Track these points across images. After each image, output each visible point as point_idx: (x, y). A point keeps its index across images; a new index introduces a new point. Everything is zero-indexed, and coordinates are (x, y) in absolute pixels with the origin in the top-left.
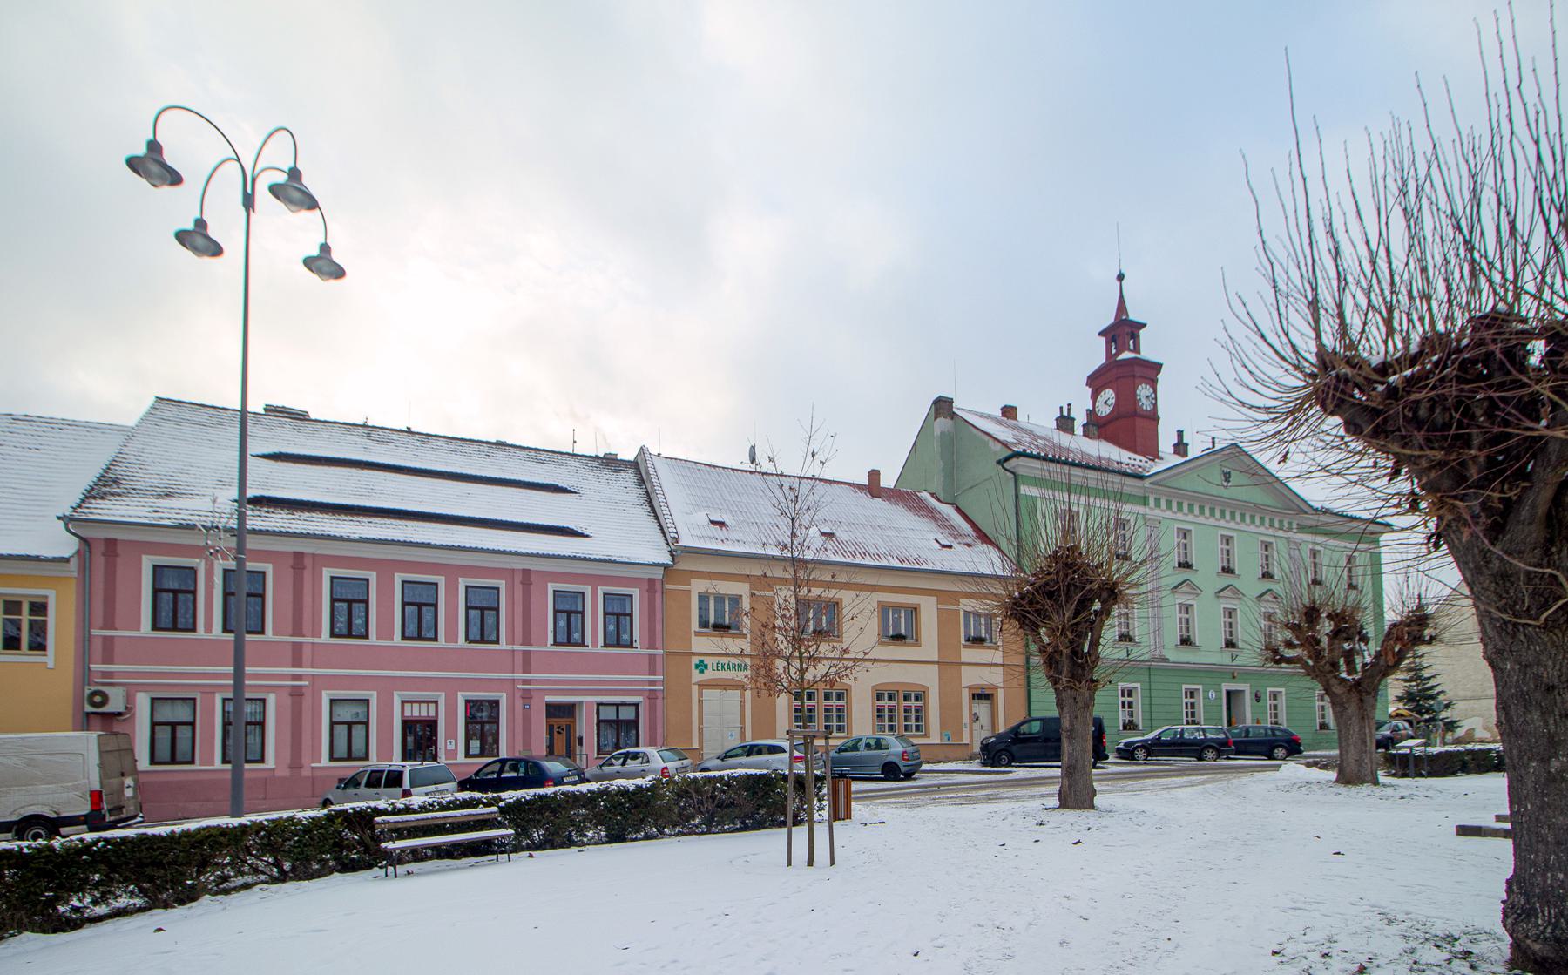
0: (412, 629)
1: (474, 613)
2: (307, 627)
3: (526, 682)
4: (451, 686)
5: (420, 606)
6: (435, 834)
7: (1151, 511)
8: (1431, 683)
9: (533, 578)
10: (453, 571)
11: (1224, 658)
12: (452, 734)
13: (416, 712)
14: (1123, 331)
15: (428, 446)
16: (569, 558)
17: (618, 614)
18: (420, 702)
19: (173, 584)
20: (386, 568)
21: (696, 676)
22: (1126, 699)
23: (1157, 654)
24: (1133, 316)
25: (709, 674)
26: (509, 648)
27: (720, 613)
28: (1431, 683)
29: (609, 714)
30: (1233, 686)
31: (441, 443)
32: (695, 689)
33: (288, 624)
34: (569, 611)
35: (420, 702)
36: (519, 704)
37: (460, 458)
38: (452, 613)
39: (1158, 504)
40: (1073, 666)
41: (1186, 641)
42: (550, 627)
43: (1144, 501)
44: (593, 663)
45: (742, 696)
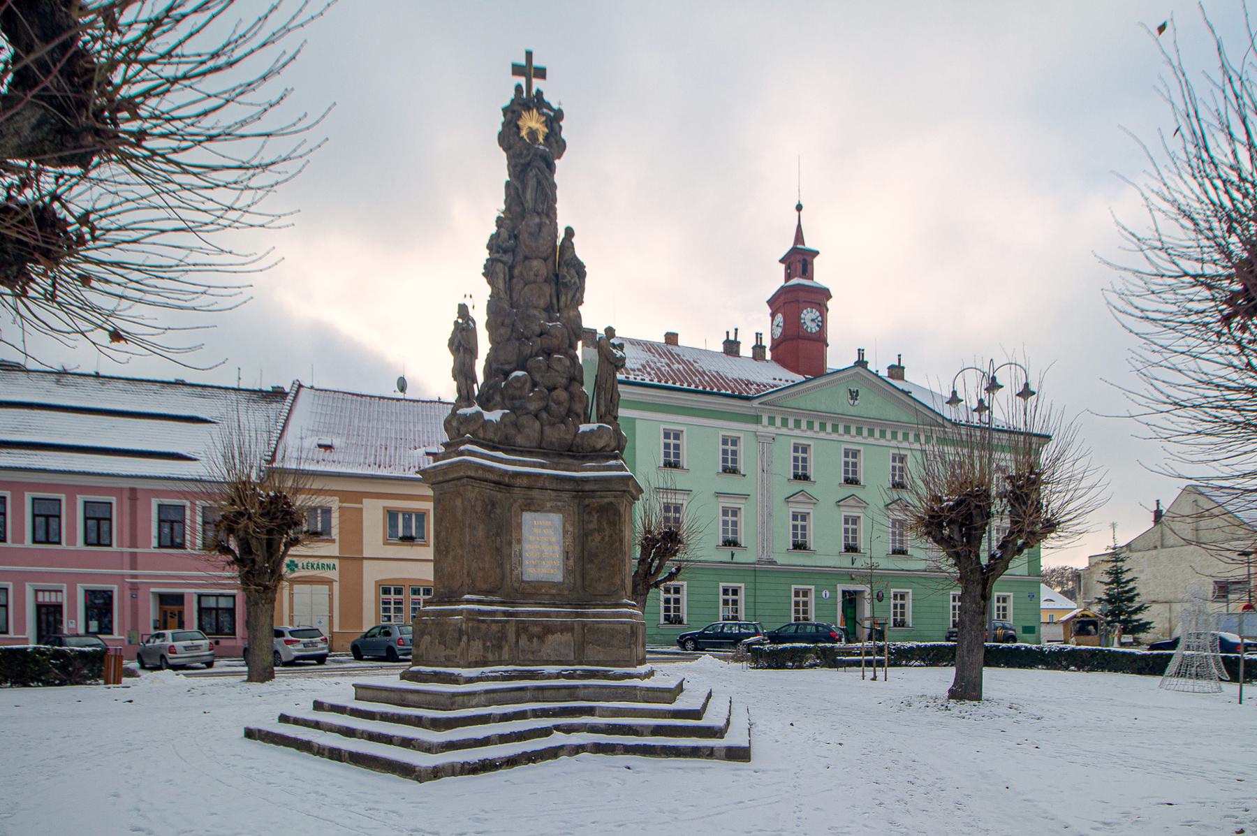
1: (40, 520)
4: (72, 579)
5: (99, 520)
6: (676, 727)
7: (764, 429)
8: (1131, 585)
9: (139, 495)
10: (72, 490)
11: (845, 561)
12: (73, 616)
14: (799, 260)
15: (107, 386)
16: (164, 478)
18: (50, 591)
22: (1001, 604)
23: (765, 557)
24: (809, 244)
25: (299, 573)
26: (119, 549)
27: (407, 525)
28: (1131, 585)
30: (851, 587)
31: (120, 385)
34: (171, 522)
35: (50, 591)
36: (127, 594)
37: (129, 396)
38: (74, 522)
39: (772, 421)
40: (978, 581)
41: (799, 546)
42: (154, 532)
43: (757, 419)
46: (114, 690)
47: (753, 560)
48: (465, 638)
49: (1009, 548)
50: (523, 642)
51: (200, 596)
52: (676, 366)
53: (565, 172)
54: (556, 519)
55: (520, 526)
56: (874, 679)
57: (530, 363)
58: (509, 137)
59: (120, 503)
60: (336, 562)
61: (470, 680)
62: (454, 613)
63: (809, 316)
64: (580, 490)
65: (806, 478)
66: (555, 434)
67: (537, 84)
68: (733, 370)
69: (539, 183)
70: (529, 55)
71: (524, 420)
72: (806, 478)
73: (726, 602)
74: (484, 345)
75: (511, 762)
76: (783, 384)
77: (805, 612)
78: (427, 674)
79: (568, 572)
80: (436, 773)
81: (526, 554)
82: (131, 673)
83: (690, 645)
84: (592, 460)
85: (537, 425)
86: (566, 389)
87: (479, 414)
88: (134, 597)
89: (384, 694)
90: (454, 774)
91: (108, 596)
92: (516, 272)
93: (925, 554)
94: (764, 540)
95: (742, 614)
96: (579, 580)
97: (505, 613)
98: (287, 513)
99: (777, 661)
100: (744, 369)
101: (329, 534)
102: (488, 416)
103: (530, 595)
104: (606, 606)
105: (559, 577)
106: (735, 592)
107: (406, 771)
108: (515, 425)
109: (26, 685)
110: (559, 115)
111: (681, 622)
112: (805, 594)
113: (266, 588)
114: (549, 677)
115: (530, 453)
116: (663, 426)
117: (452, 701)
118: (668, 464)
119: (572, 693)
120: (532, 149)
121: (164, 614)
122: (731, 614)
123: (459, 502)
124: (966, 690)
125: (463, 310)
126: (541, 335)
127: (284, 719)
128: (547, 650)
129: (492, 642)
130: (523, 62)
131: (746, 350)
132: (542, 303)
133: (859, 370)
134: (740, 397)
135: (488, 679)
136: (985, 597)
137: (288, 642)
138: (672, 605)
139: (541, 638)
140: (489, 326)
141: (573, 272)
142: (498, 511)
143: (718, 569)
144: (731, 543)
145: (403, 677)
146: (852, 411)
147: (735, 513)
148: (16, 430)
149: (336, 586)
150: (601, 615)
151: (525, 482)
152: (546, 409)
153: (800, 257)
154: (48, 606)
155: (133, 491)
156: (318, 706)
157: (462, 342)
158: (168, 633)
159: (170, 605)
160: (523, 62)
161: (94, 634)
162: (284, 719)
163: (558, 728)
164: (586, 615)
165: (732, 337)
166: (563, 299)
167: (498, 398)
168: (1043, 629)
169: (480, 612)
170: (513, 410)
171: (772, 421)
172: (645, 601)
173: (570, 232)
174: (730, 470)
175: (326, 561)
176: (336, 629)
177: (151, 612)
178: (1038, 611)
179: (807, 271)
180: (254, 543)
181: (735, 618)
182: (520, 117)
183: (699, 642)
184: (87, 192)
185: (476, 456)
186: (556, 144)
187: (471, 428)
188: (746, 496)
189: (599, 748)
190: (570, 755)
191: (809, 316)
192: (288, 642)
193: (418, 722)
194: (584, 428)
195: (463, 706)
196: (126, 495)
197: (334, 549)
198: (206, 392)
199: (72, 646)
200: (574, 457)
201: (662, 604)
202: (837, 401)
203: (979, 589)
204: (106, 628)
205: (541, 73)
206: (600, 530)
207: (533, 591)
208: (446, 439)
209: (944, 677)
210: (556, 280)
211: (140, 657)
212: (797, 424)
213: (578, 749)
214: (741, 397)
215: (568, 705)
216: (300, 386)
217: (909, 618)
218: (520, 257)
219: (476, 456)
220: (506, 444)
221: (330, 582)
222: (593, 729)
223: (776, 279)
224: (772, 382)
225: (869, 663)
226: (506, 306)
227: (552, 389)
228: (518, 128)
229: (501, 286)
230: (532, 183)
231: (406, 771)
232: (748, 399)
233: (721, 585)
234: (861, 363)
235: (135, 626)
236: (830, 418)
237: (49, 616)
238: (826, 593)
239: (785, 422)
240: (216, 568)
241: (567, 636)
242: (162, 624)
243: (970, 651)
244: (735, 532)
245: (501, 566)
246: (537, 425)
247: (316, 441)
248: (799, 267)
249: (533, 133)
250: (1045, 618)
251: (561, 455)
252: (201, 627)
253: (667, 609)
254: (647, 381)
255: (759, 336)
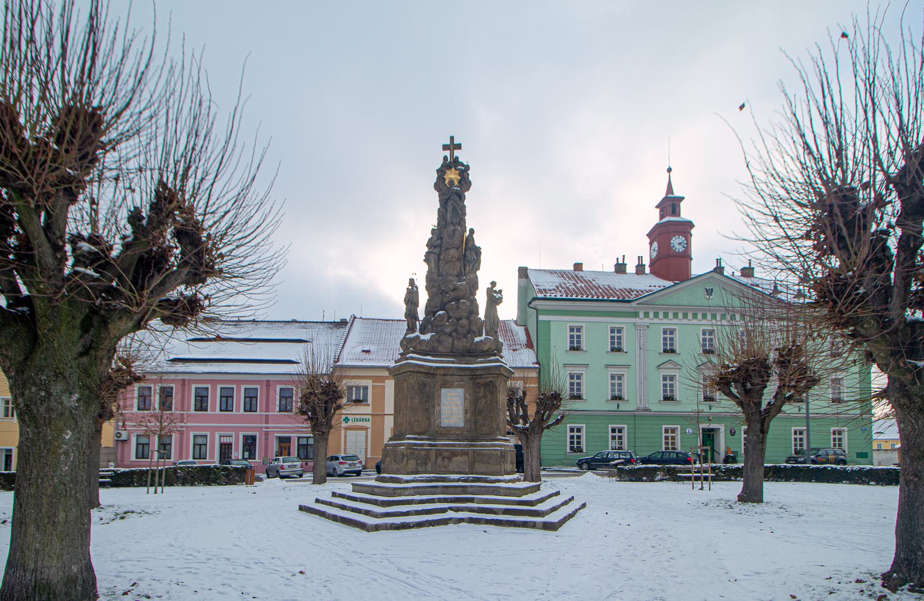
0: (224, 407)
1: (224, 399)
2: (186, 408)
3: (267, 428)
5: (251, 398)
7: (641, 320)
12: (237, 450)
13: (224, 440)
14: (670, 204)
17: (166, 394)
19: (287, 395)
20: (214, 382)
21: (344, 424)
23: (642, 407)
24: (677, 193)
25: (350, 423)
27: (358, 393)
29: (304, 442)
32: (343, 432)
33: (179, 408)
36: (263, 437)
38: (239, 399)
39: (646, 315)
40: (759, 420)
41: (668, 398)
42: (278, 403)
43: (635, 315)
44: (240, 419)
45: (367, 433)
46: (250, 488)
47: (634, 408)
48: (405, 459)
49: (780, 399)
50: (439, 461)
51: (299, 438)
52: (580, 284)
53: (470, 199)
54: (460, 391)
55: (440, 396)
56: (702, 489)
57: (447, 306)
58: (440, 185)
59: (261, 388)
60: (370, 417)
61: (407, 481)
62: (401, 445)
63: (677, 242)
64: (474, 375)
65: (673, 351)
66: (460, 344)
67: (457, 153)
68: (620, 283)
69: (454, 208)
70: (452, 138)
71: (443, 338)
72: (673, 351)
73: (613, 438)
74: (423, 298)
75: (420, 525)
76: (656, 289)
77: (673, 444)
78: (387, 478)
79: (466, 421)
80: (377, 528)
81: (443, 412)
82: (260, 480)
83: (585, 466)
84: (482, 357)
85: (450, 339)
86: (468, 318)
87: (418, 337)
88: (266, 439)
89: (365, 489)
90: (386, 529)
91: (254, 438)
92: (442, 257)
93: (726, 405)
94: (644, 393)
95: (625, 446)
96: (473, 425)
97: (430, 445)
98: (335, 392)
99: (635, 476)
100: (631, 282)
101: (367, 401)
102: (423, 337)
103: (445, 435)
104: (487, 441)
105: (462, 424)
106: (620, 431)
107: (362, 526)
108: (438, 341)
109: (209, 485)
110: (467, 168)
111: (581, 451)
112: (673, 431)
113: (323, 433)
114: (453, 481)
115: (446, 356)
116: (569, 324)
117: (394, 492)
118: (572, 348)
119: (464, 490)
120: (453, 185)
121: (281, 448)
122: (617, 446)
123: (405, 385)
124: (751, 495)
125: (412, 282)
126: (454, 290)
127: (317, 501)
128: (452, 466)
129: (421, 461)
130: (448, 143)
131: (631, 268)
132: (455, 273)
133: (716, 276)
134: (624, 301)
135: (418, 481)
136: (764, 431)
137: (341, 463)
138: (575, 440)
139: (450, 459)
140: (427, 288)
141: (473, 253)
142: (427, 389)
143: (606, 416)
144: (617, 398)
145: (376, 480)
146: (706, 303)
147: (620, 378)
148: (215, 352)
149: (370, 431)
150: (485, 446)
151: (442, 372)
152: (456, 330)
153: (670, 203)
154: (225, 444)
155: (268, 381)
156: (334, 494)
157: (411, 298)
158: (281, 458)
159: (284, 442)
160: (448, 143)
161: (246, 459)
162: (317, 501)
163: (451, 508)
164: (476, 446)
165: (620, 262)
166: (467, 268)
167: (429, 327)
168: (875, 455)
169: (415, 444)
170: (437, 333)
171: (646, 315)
172: (540, 437)
173: (472, 231)
174: (616, 349)
175: (364, 417)
176: (369, 456)
177: (274, 446)
178: (870, 441)
179: (675, 211)
180: (318, 409)
181: (620, 448)
182: (445, 173)
183: (593, 464)
184: (209, 288)
185: (416, 360)
186: (465, 182)
187: (413, 345)
188: (628, 366)
189: (472, 521)
190: (455, 523)
191: (677, 242)
192: (341, 463)
193: (375, 502)
194: (477, 339)
195: (400, 495)
196: (265, 383)
197: (368, 410)
198: (306, 325)
199: (235, 464)
200: (471, 356)
201: (568, 440)
202: (698, 298)
203: (759, 426)
204: (252, 456)
205: (459, 147)
206: (485, 397)
207: (447, 433)
208: (402, 351)
209: (736, 487)
210: (464, 259)
211: (267, 472)
212: (666, 315)
213: (460, 520)
214: (623, 302)
215: (460, 496)
216: (355, 317)
217: (584, 445)
218: (444, 248)
219: (416, 360)
220: (434, 352)
221: (366, 429)
222: (471, 510)
223: (653, 218)
224: (648, 288)
225: (697, 479)
226: (435, 277)
227: (459, 319)
228: (444, 179)
229: (433, 265)
230: (450, 208)
231: (362, 526)
232: (628, 302)
233: (610, 426)
234: (719, 270)
235: (266, 455)
236: (662, 309)
237: (225, 449)
238: (689, 430)
239: (656, 315)
240: (299, 423)
241: (465, 458)
242: (280, 453)
243: (752, 469)
244: (620, 390)
245: (429, 419)
246: (450, 339)
247: (360, 348)
248: (670, 209)
249: (451, 182)
250: (875, 447)
251: (464, 356)
252: (298, 455)
253: (572, 443)
254: (558, 297)
255: (640, 258)
